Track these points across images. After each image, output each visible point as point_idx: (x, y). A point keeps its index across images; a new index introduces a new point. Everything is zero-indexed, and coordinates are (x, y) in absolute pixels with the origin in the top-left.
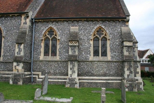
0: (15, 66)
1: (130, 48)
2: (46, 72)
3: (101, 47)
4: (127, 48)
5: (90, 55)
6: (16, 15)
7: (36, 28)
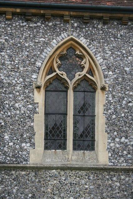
5: (33, 145)
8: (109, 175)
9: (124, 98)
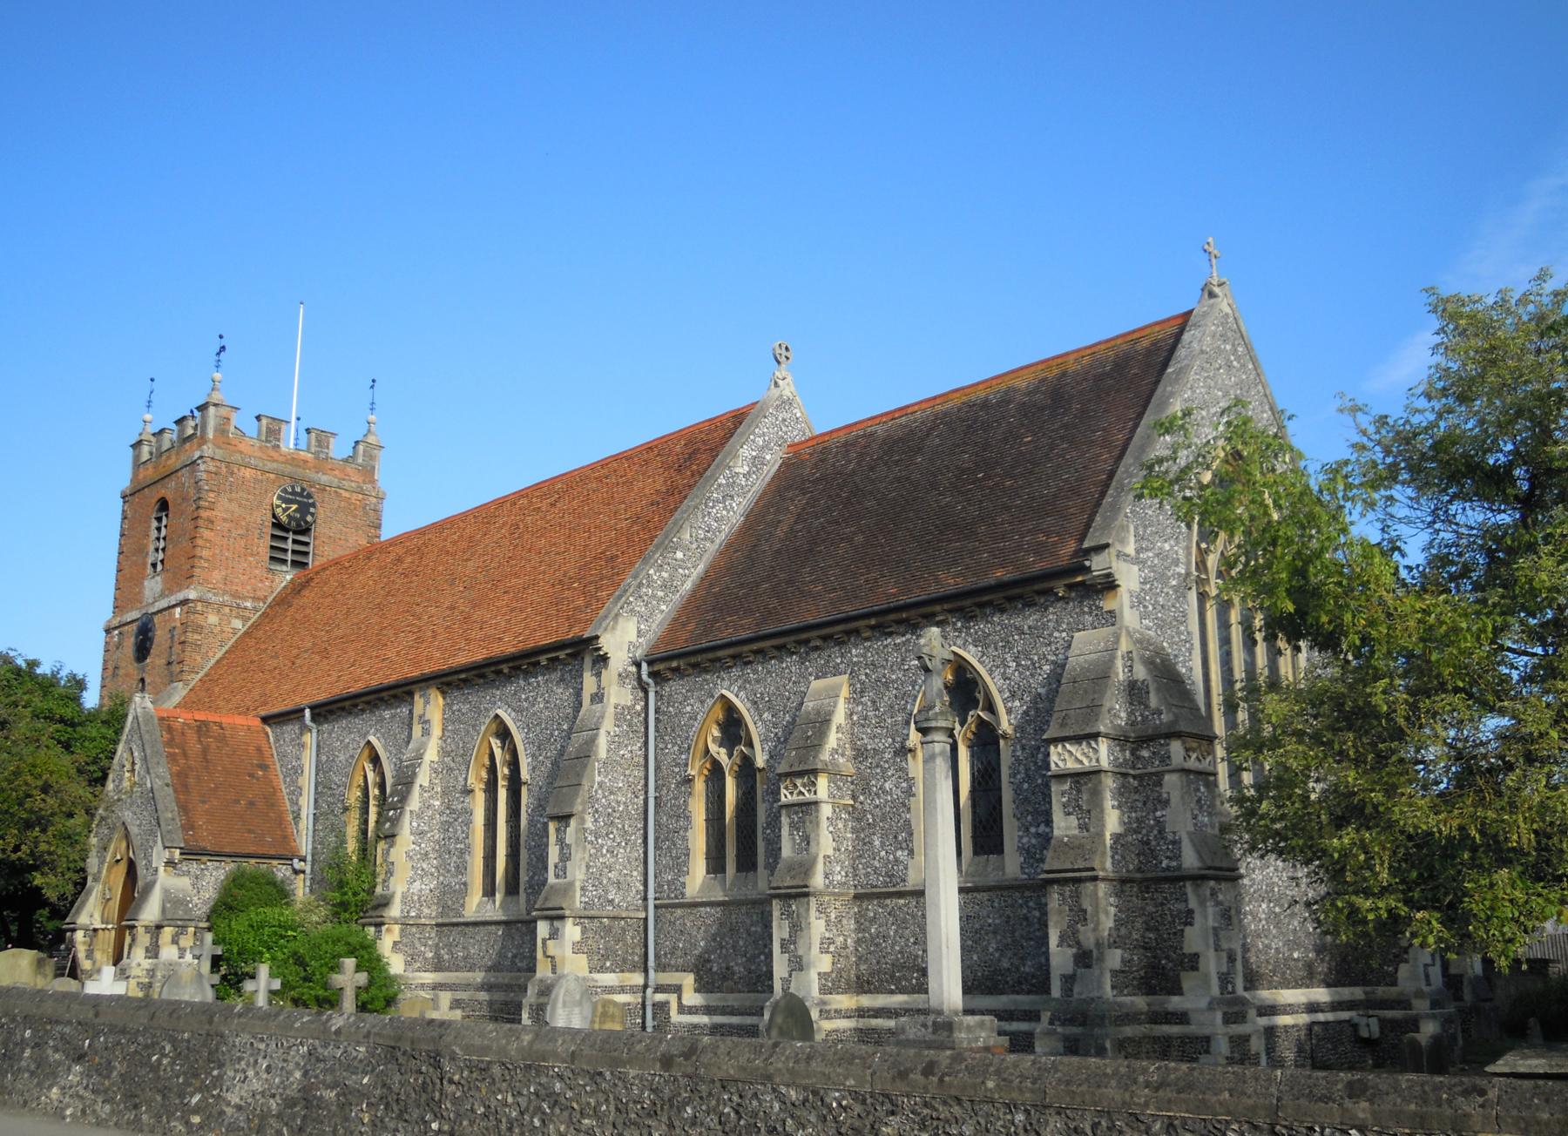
0: (544, 941)
1: (1083, 788)
2: (715, 969)
3: (703, 824)
4: (1066, 787)
5: (911, 853)
6: (562, 654)
7: (664, 713)
8: (1022, 897)
9: (1039, 748)
